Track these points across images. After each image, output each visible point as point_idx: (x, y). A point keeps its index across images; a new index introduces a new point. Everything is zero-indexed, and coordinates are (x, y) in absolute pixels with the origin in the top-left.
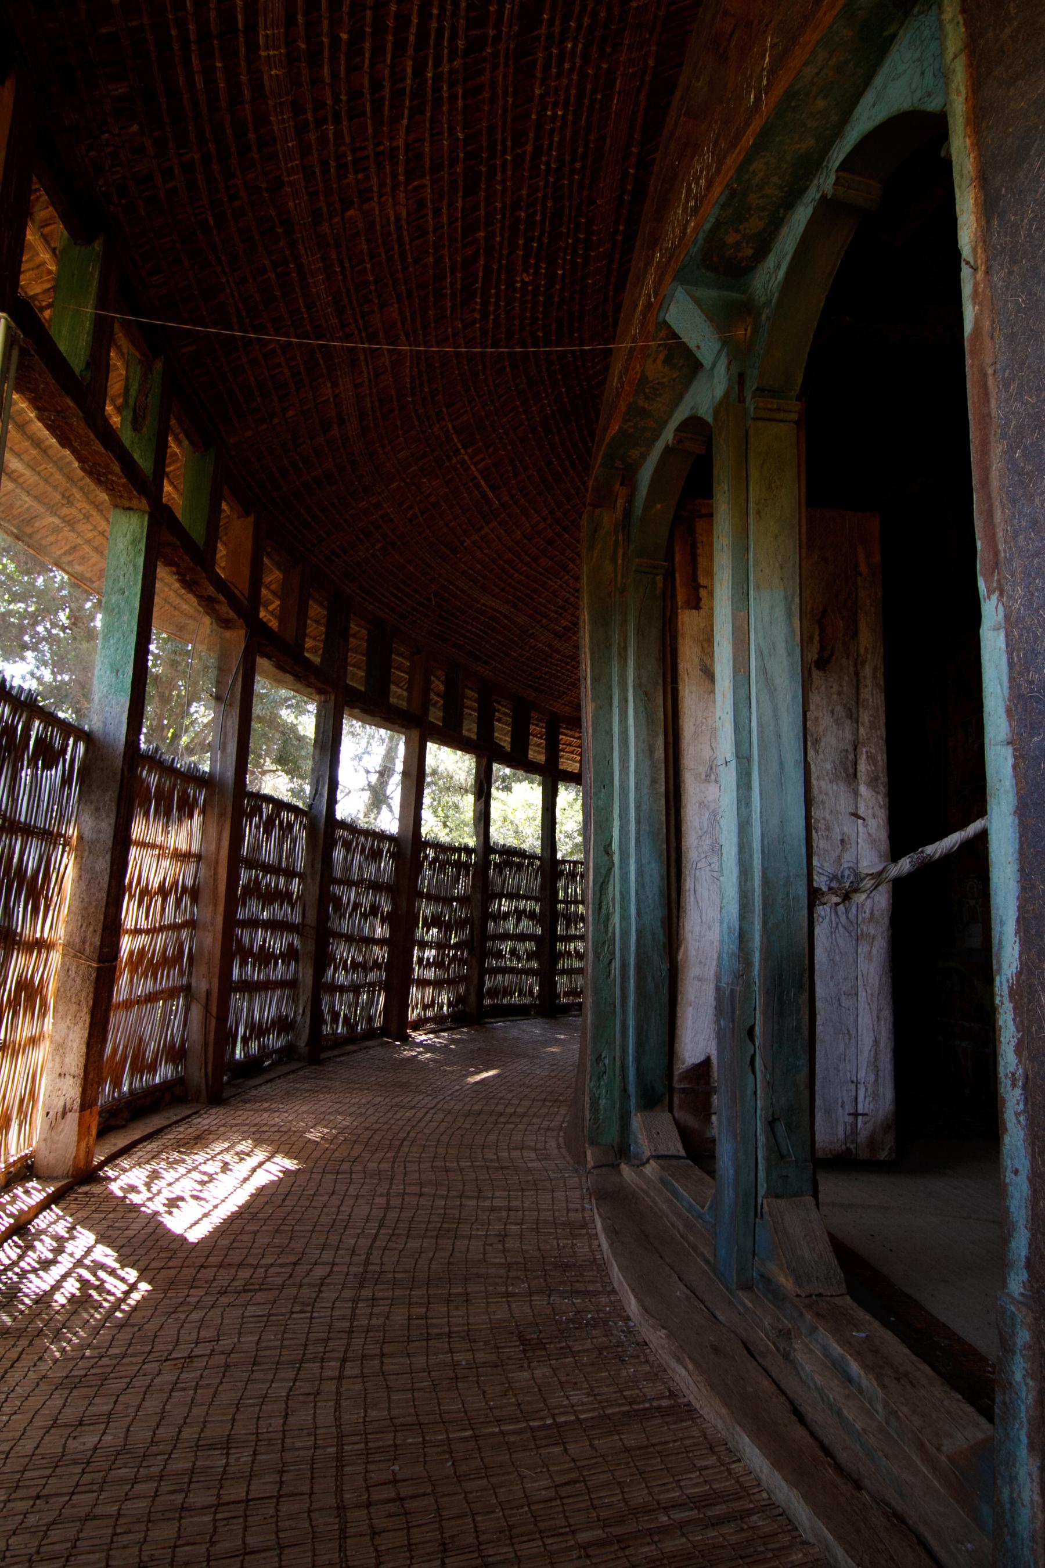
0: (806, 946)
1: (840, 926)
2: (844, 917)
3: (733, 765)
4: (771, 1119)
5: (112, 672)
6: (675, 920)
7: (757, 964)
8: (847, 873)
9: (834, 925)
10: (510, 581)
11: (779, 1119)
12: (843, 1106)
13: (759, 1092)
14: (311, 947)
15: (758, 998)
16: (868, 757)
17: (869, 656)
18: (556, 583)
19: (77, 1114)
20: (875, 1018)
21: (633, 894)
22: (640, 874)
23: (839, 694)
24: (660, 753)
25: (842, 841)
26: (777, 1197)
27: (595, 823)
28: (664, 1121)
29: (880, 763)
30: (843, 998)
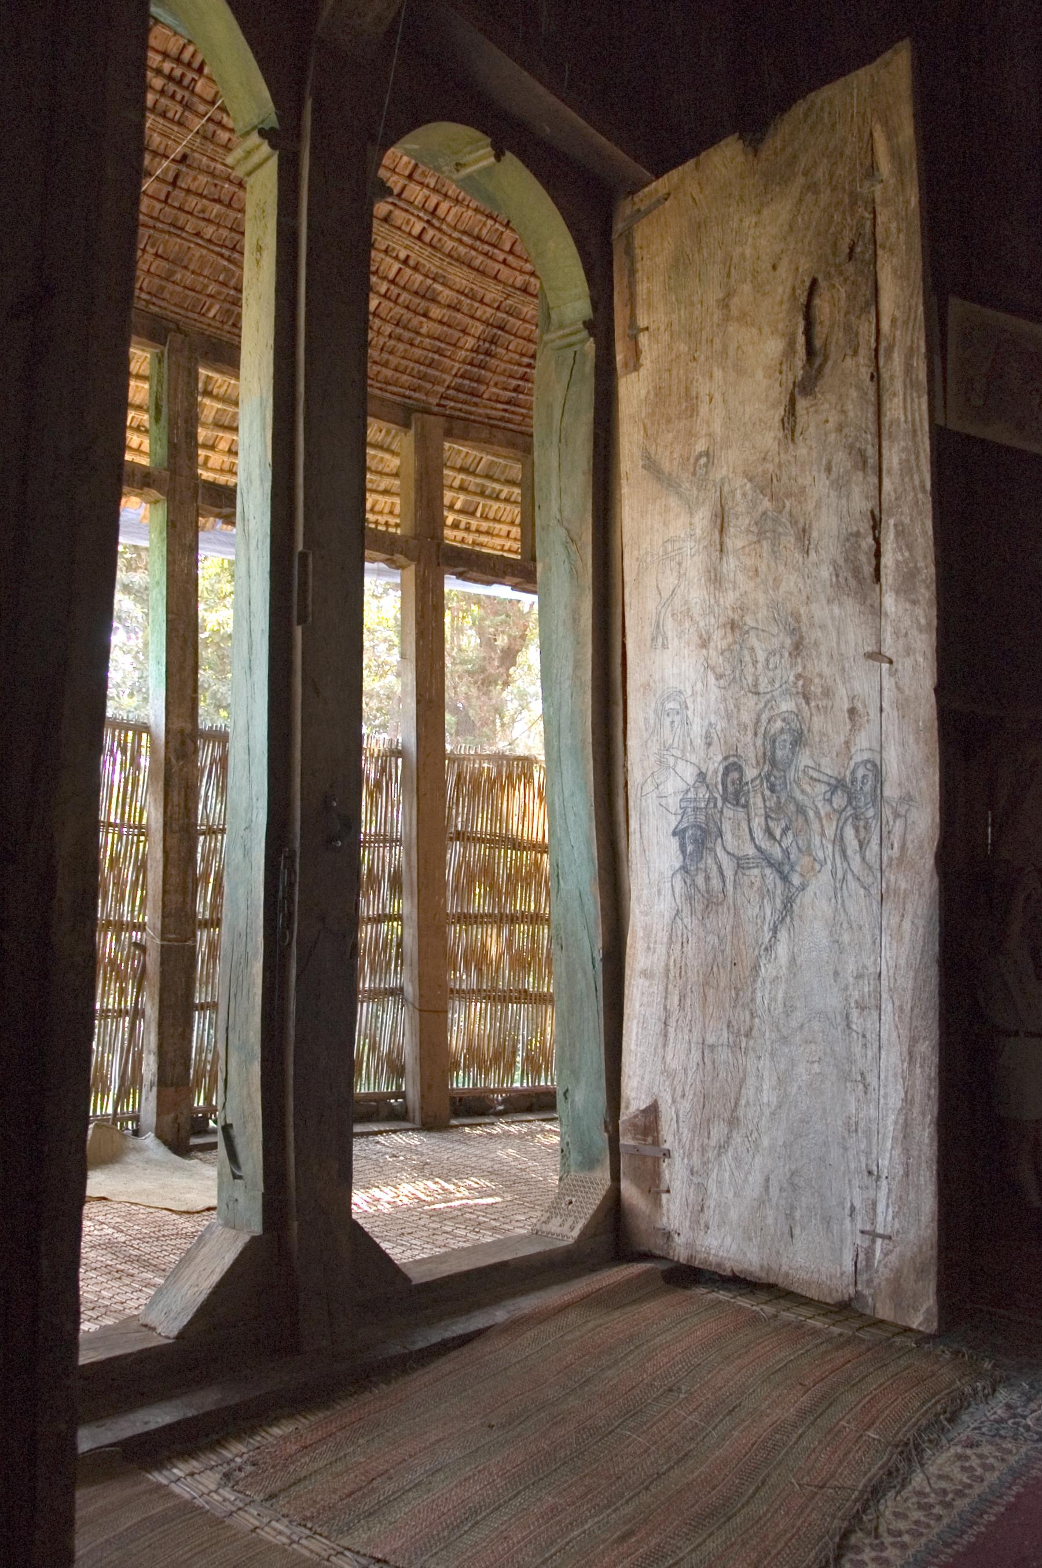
8: (860, 773)
9: (840, 875)
16: (898, 534)
25: (852, 712)
30: (855, 1014)
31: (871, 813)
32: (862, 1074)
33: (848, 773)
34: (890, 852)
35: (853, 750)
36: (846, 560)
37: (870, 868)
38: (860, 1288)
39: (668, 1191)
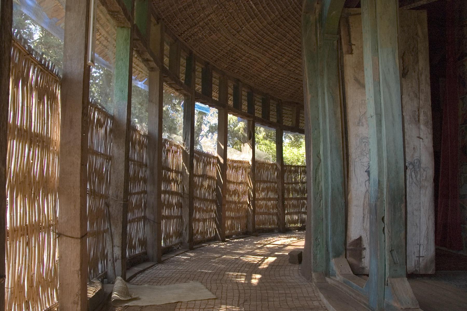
0: (404, 186)
1: (413, 183)
2: (415, 179)
3: (374, 117)
4: (391, 250)
5: (120, 92)
6: (346, 183)
7: (385, 194)
8: (416, 161)
9: (411, 182)
10: (261, 43)
11: (394, 250)
12: (414, 254)
13: (386, 240)
14: (187, 202)
15: (386, 206)
16: (424, 113)
17: (424, 71)
18: (281, 43)
19: (121, 260)
20: (427, 219)
21: (330, 173)
22: (332, 165)
23: (412, 87)
24: (339, 115)
25: (414, 148)
26: (393, 277)
27: (313, 144)
28: (343, 261)
29: (429, 115)
30: (415, 212)
31: (418, 170)
32: (416, 224)
33: (413, 161)
34: (423, 178)
35: (414, 156)
36: (413, 116)
37: (418, 181)
38: (416, 268)
39: (364, 258)
